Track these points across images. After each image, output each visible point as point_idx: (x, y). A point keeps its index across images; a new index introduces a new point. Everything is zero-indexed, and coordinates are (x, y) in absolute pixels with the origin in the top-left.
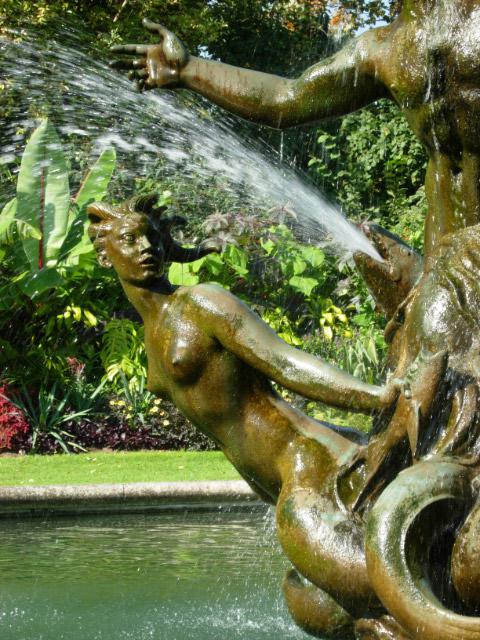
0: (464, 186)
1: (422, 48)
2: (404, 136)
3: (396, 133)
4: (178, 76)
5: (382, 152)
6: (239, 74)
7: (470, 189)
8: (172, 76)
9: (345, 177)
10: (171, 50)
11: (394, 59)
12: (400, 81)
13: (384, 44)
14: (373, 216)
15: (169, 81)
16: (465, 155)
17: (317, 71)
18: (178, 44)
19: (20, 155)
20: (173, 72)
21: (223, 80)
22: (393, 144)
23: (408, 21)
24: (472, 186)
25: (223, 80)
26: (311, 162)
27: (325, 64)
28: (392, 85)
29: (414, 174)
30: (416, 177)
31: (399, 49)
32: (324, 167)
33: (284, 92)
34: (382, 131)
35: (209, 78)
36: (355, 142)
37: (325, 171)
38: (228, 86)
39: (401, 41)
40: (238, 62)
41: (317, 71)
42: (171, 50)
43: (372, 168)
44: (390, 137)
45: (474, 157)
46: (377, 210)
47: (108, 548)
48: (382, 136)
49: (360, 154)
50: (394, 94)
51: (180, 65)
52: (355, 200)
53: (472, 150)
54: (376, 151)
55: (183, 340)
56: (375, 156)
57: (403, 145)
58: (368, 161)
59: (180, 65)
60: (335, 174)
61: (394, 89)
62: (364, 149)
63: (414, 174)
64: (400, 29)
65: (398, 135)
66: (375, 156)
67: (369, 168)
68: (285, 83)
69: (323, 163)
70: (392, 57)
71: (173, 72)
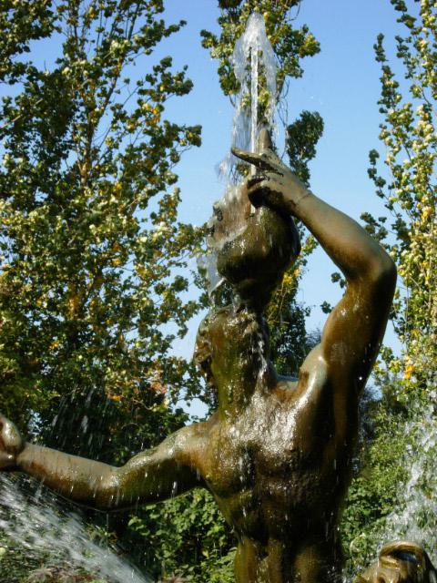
0: (270, 569)
1: (235, 443)
2: (214, 503)
3: (207, 500)
4: (14, 460)
5: (193, 517)
6: (70, 460)
7: (274, 571)
8: (8, 461)
9: (163, 536)
10: (9, 437)
11: (210, 452)
12: (214, 474)
13: (200, 439)
14: (186, 573)
15: (6, 465)
16: (271, 541)
17: (140, 460)
18: (16, 432)
19: (186, 323)
20: (10, 457)
21: (54, 465)
22: (204, 510)
23: (223, 419)
24: (277, 567)
25: (54, 465)
26: (131, 522)
27: (147, 454)
28: (208, 476)
29: (222, 538)
30: (224, 541)
31: (214, 443)
32: (142, 526)
33: (111, 479)
34: (194, 497)
35: (42, 463)
36: (170, 506)
37: (143, 530)
38: (59, 471)
39: (215, 437)
40: (69, 449)
41: (140, 460)
42: (9, 437)
43: (184, 531)
44: (202, 503)
45: (278, 543)
46: (191, 569)
47: (121, 425)
48: (194, 501)
49: (173, 517)
50: (209, 485)
51: (17, 450)
52: (171, 557)
53: (278, 537)
54: (188, 515)
55: (106, 476)
56: (187, 520)
57: (213, 512)
58: (181, 524)
59: (17, 450)
60: (153, 533)
61: (209, 480)
62: (177, 512)
63: (222, 538)
64: (215, 426)
65: (209, 502)
66: (187, 520)
67: (180, 531)
68: (111, 470)
69: (142, 523)
70: (207, 450)
71: (10, 457)
